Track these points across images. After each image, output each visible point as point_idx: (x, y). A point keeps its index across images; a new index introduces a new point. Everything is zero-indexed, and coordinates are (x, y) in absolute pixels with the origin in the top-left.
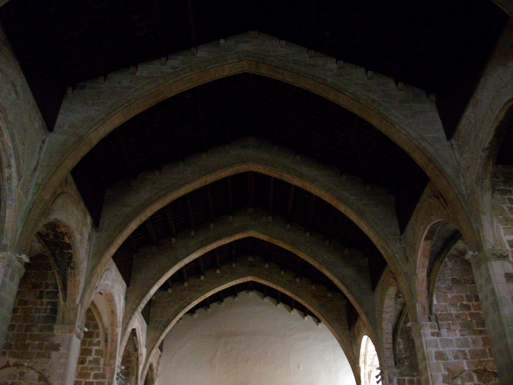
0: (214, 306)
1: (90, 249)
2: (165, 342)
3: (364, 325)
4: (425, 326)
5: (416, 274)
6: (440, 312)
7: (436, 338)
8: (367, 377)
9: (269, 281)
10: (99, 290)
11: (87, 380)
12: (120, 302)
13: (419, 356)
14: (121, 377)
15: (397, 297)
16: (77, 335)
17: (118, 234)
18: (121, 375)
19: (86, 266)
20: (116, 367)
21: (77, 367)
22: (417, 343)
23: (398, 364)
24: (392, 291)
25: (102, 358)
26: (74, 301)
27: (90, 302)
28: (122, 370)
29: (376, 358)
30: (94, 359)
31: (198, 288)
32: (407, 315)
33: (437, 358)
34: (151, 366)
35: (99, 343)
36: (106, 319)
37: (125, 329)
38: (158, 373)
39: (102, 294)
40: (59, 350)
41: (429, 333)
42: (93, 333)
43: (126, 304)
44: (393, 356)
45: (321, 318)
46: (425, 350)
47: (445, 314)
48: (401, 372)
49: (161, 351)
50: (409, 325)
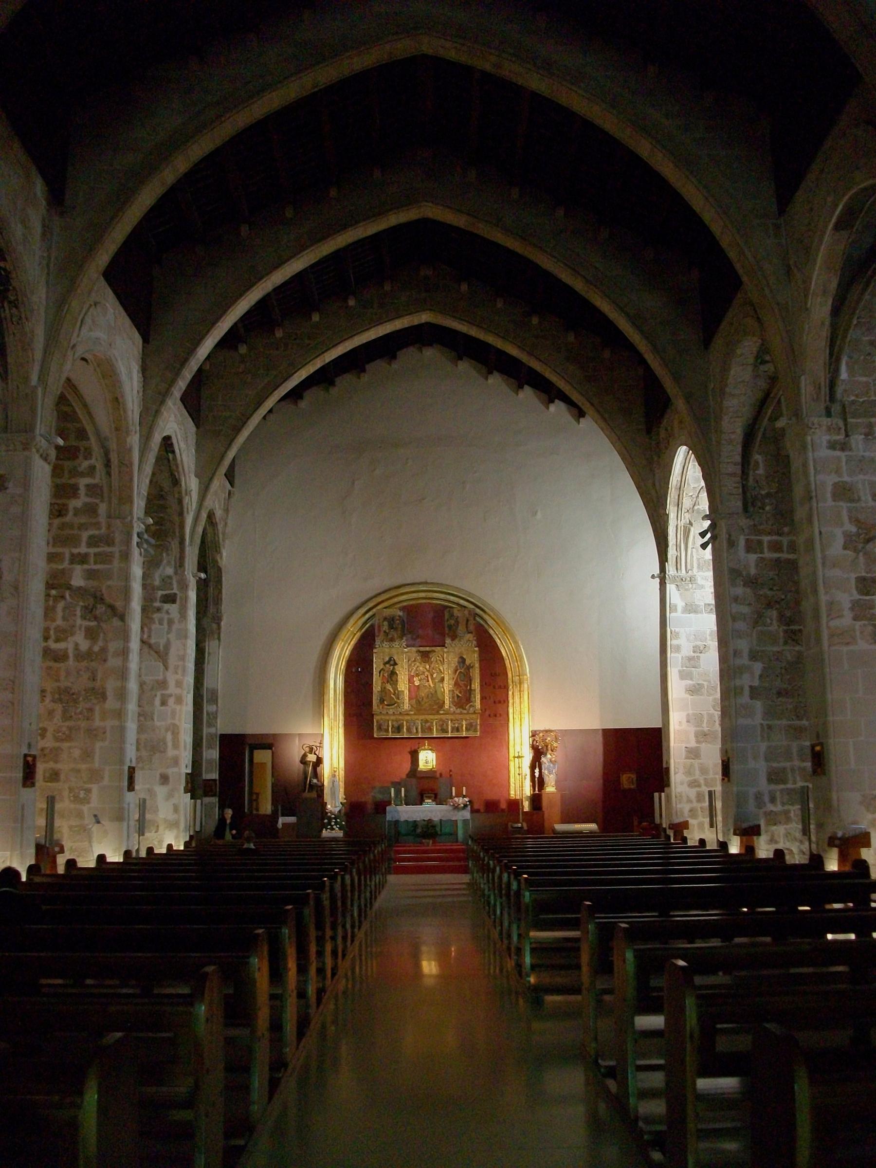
0: (345, 381)
1: (49, 257)
2: (236, 461)
3: (681, 422)
4: (817, 426)
5: (807, 309)
6: (853, 398)
7: (838, 453)
8: (681, 535)
10: (80, 351)
11: (75, 551)
12: (131, 378)
13: (798, 491)
14: (147, 541)
15: (759, 361)
16: (41, 456)
17: (112, 219)
18: (146, 536)
19: (44, 296)
20: (135, 519)
21: (50, 524)
22: (796, 464)
23: (751, 509)
24: (748, 347)
25: (102, 501)
26: (27, 379)
27: (63, 379)
28: (148, 527)
29: (704, 495)
30: (86, 504)
31: (307, 342)
32: (779, 402)
33: (836, 496)
34: (211, 516)
35: (92, 468)
36: (103, 417)
37: (146, 438)
38: (229, 530)
39: (89, 361)
40: (6, 489)
41: (825, 444)
42: (77, 449)
43: (144, 381)
45: (586, 406)
46: (812, 479)
47: (864, 401)
48: (755, 525)
49: (232, 484)
50: (780, 423)
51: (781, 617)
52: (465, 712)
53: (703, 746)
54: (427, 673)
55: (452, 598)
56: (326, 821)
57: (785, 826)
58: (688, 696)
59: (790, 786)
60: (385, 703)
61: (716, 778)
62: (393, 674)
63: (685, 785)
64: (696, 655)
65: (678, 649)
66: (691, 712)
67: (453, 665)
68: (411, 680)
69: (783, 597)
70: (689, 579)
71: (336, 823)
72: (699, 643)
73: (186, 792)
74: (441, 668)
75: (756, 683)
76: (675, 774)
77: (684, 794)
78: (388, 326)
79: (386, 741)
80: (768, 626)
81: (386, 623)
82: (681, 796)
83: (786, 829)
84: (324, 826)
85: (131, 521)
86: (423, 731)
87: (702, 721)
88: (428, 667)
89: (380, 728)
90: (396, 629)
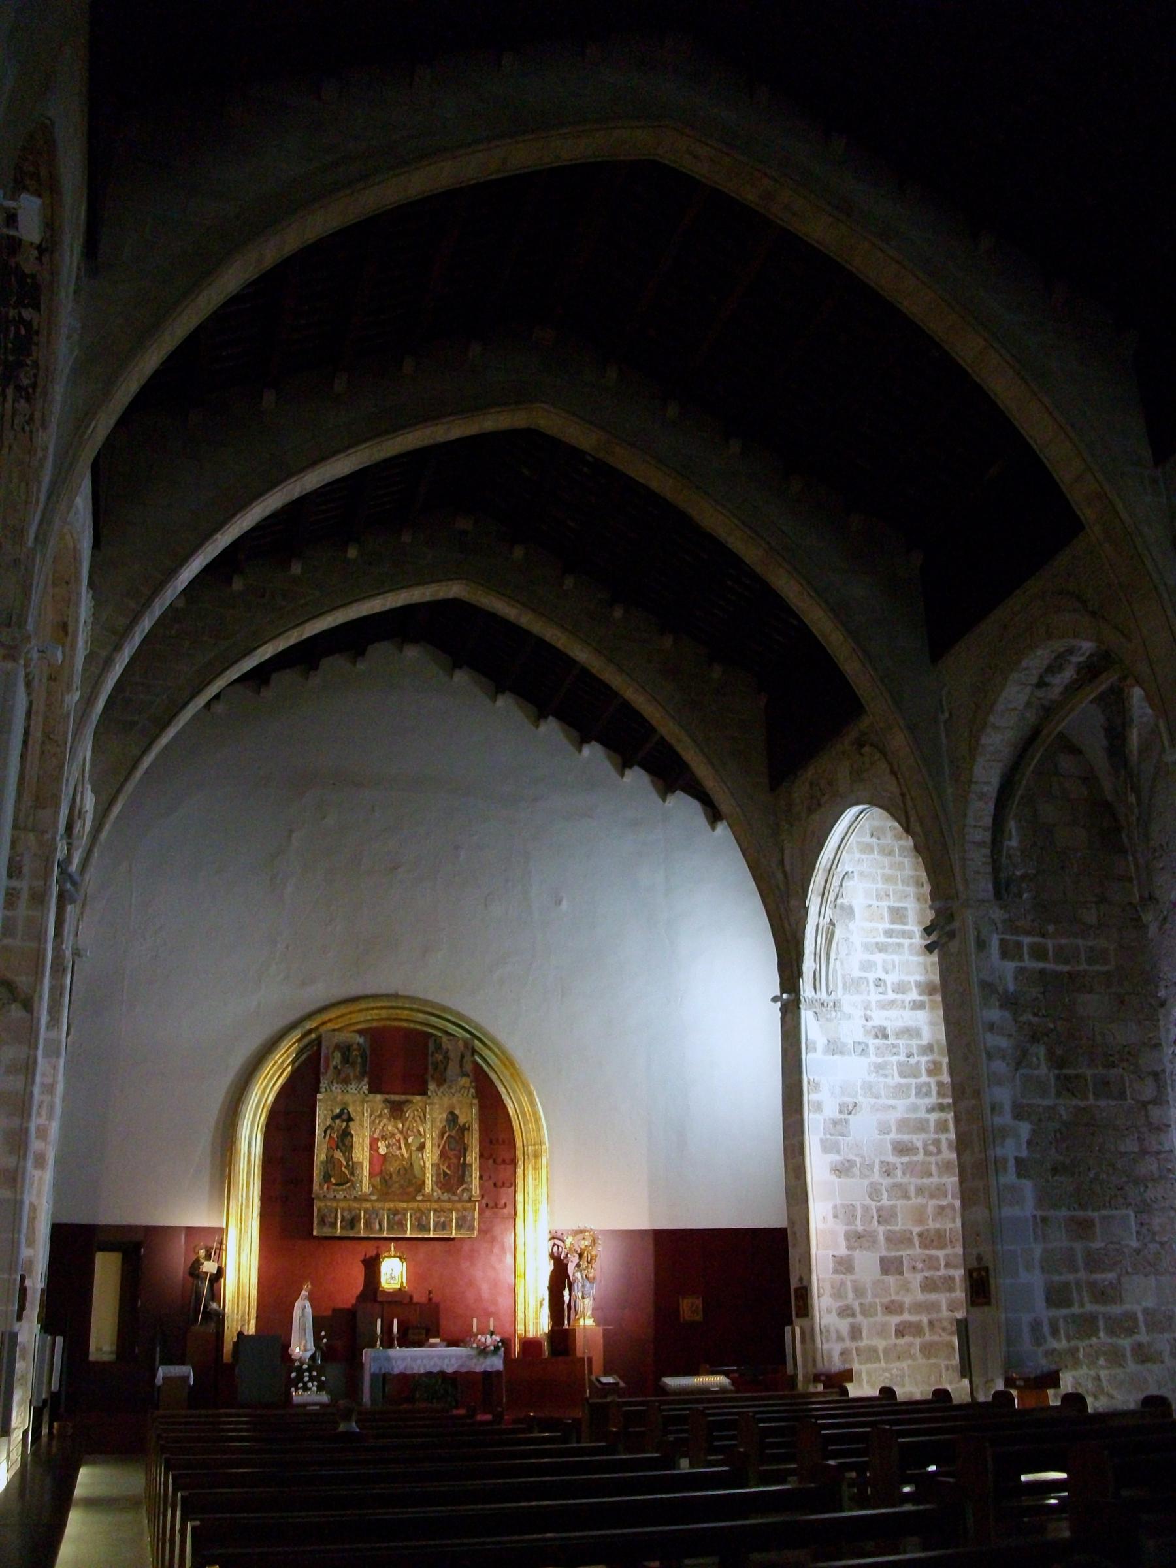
0: (335, 665)
8: (821, 939)
9: (523, 605)
44: (989, 869)
51: (1050, 1053)
52: (456, 1198)
53: (857, 1254)
54: (398, 1136)
55: (433, 1020)
56: (293, 1375)
57: (1074, 1373)
58: (834, 1178)
59: (1076, 1309)
60: (333, 1180)
61: (875, 1303)
62: (346, 1134)
63: (834, 1313)
64: (843, 1116)
65: (819, 1107)
66: (838, 1202)
67: (440, 1125)
68: (373, 1146)
69: (1052, 1026)
70: (832, 1004)
71: (312, 1379)
72: (847, 1099)
73: (38, 1323)
74: (421, 1130)
75: (1024, 1154)
76: (819, 1297)
77: (832, 1329)
78: (403, 596)
79: (348, 1243)
80: (1035, 1069)
81: (338, 1055)
82: (828, 1331)
83: (1074, 1377)
84: (294, 1383)
85: (54, 839)
86: (390, 1228)
87: (854, 1216)
88: (400, 1126)
89: (322, 1222)
90: (353, 1064)
